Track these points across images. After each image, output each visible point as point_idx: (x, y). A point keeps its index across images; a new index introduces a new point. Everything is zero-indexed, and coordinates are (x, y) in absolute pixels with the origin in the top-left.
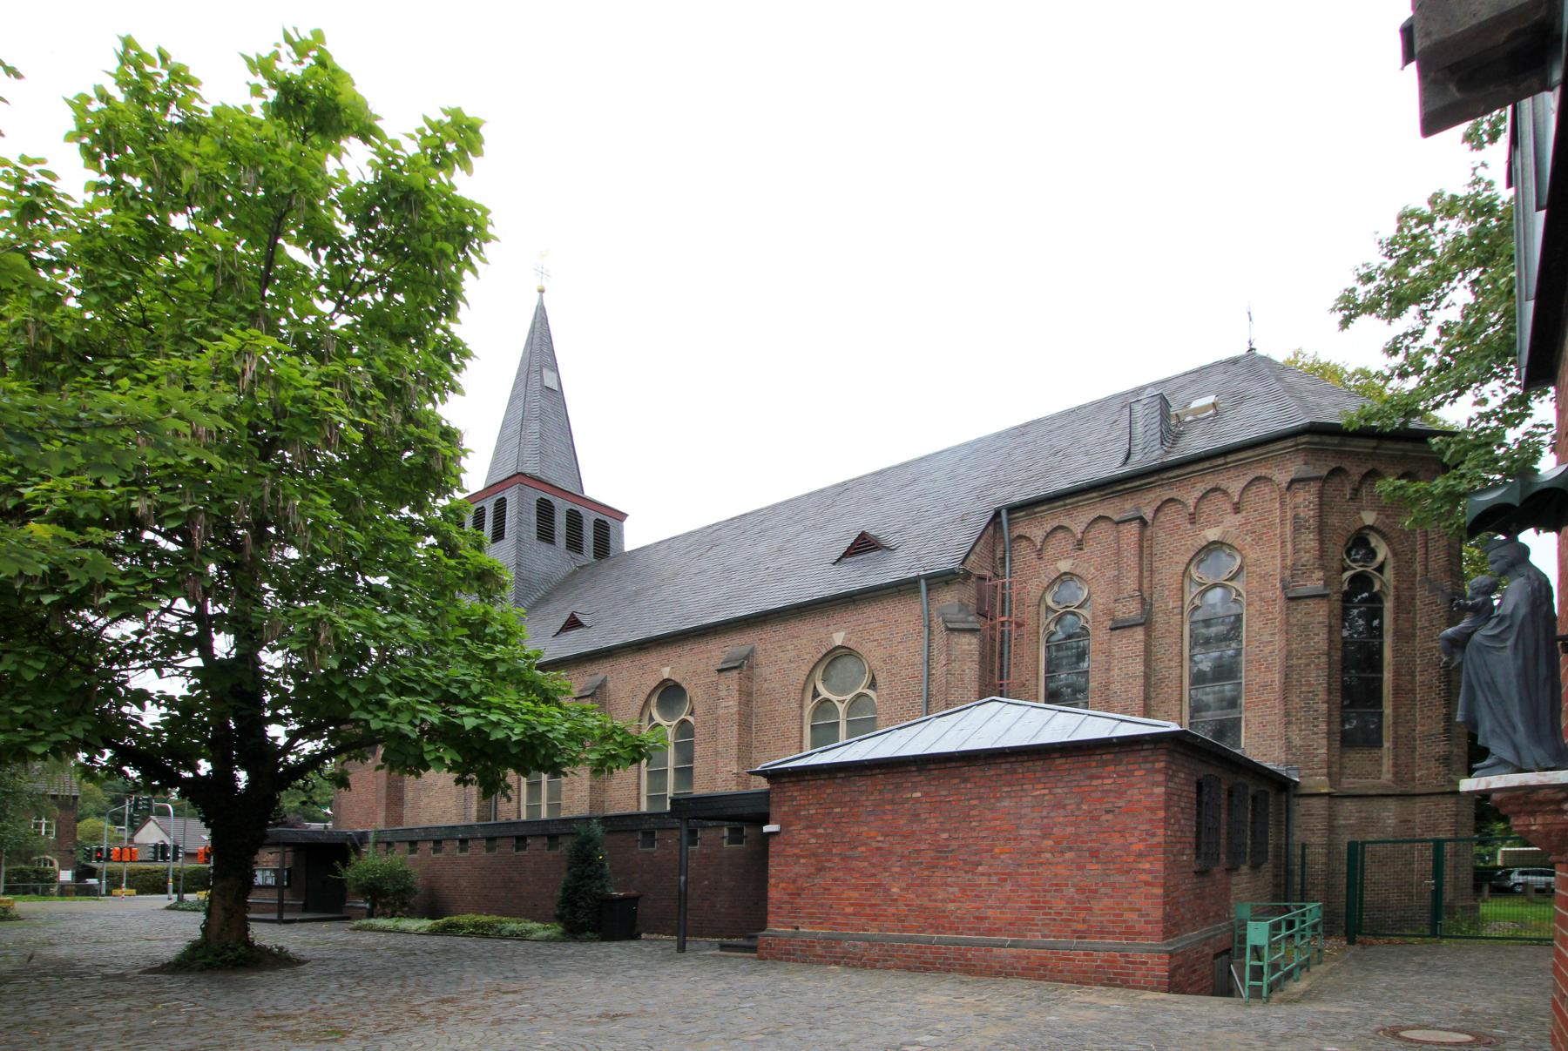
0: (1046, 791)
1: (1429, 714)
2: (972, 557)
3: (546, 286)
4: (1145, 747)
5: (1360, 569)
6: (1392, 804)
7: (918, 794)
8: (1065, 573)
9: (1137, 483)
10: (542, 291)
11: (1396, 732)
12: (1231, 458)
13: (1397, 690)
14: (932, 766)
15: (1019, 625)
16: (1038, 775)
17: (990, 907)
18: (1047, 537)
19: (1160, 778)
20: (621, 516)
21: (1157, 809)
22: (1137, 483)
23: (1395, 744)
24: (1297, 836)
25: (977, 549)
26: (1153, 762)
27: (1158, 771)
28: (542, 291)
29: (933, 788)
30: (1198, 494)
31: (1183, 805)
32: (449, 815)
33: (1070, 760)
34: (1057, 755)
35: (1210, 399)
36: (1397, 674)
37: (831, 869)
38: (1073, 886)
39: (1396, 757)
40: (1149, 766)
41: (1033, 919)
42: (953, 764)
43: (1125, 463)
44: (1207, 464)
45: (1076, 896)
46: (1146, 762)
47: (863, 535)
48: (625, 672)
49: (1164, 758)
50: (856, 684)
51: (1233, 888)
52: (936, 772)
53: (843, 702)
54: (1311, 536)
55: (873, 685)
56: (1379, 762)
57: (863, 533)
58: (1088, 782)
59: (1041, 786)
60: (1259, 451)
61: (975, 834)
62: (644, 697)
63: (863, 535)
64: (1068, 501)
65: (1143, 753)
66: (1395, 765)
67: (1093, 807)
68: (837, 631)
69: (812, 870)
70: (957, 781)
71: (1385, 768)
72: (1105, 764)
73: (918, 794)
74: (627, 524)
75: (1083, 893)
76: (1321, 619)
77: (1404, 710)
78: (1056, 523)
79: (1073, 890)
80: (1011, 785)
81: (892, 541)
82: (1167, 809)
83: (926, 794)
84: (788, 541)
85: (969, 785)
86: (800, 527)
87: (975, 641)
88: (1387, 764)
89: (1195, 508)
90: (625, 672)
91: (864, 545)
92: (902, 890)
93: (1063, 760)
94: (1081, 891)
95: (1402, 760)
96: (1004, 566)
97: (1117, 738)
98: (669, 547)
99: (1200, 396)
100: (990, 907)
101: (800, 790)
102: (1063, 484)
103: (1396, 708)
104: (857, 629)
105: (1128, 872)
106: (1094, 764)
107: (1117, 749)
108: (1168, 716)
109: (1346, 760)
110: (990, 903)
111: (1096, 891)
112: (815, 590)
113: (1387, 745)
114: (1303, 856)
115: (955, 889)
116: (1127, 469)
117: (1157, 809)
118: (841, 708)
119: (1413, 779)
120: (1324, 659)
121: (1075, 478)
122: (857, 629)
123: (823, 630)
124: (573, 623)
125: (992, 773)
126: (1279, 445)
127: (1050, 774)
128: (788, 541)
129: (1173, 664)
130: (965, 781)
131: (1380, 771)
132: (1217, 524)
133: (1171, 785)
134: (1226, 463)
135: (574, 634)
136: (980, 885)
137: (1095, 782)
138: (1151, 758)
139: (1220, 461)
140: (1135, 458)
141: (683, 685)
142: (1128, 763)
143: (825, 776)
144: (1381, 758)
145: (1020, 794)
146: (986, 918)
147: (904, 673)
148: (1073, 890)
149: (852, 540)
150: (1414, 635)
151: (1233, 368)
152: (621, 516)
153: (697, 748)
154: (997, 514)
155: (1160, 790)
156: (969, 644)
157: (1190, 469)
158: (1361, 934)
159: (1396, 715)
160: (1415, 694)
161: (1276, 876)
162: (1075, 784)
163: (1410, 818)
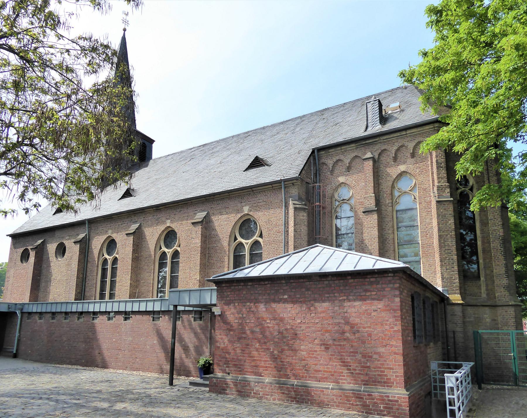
0: (345, 298)
1: (498, 263)
2: (303, 172)
3: (126, 27)
4: (389, 275)
5: (464, 189)
6: (487, 310)
7: (286, 297)
8: (342, 183)
9: (396, 135)
10: (125, 30)
11: (485, 272)
12: (408, 132)
13: (484, 251)
14: (292, 281)
15: (323, 208)
16: (341, 288)
17: (321, 365)
18: (334, 164)
19: (397, 293)
20: (152, 141)
21: (397, 310)
22: (371, 141)
23: (486, 278)
24: (450, 326)
25: (305, 168)
26: (394, 284)
27: (396, 289)
28: (125, 30)
29: (293, 293)
30: (395, 148)
31: (407, 308)
32: (61, 297)
33: (356, 280)
34: (349, 277)
35: (397, 104)
36: (483, 243)
37: (245, 338)
38: (361, 353)
39: (487, 285)
40: (391, 285)
41: (342, 373)
42: (302, 280)
43: (366, 131)
44: (398, 134)
45: (363, 360)
46: (391, 284)
47: (257, 158)
48: (150, 222)
49: (398, 281)
50: (253, 235)
51: (429, 356)
52: (294, 284)
53: (247, 244)
54: (443, 172)
55: (261, 236)
56: (479, 287)
57: (257, 157)
58: (364, 294)
59: (343, 294)
60: (419, 129)
61: (313, 321)
62: (158, 236)
63: (257, 158)
64: (343, 148)
65: (389, 278)
66: (487, 290)
67: (367, 308)
68: (245, 205)
69: (236, 339)
70: (304, 290)
71: (482, 291)
72: (371, 283)
73: (286, 297)
74: (154, 145)
75: (365, 358)
76: (450, 213)
77: (488, 261)
78: (338, 158)
79: (360, 355)
80: (329, 294)
81: (269, 161)
82: (401, 311)
83: (290, 296)
84: (224, 159)
85: (309, 293)
86: (229, 152)
87: (305, 214)
88: (483, 289)
89: (395, 155)
90: (150, 222)
91: (257, 163)
92: (279, 352)
93: (352, 280)
94: (364, 356)
95: (490, 287)
96: (317, 177)
97: (377, 269)
98: (172, 158)
99: (394, 102)
100: (321, 365)
101: (231, 292)
102: (340, 139)
103: (484, 260)
104: (254, 205)
105: (385, 346)
106: (367, 283)
107: (377, 276)
108: (399, 258)
109: (466, 286)
110: (321, 362)
111: (371, 357)
112: (235, 184)
113: (482, 279)
114: (454, 337)
115: (305, 353)
116: (366, 133)
117: (397, 310)
118: (247, 247)
119: (495, 298)
120: (453, 233)
121: (345, 137)
122: (254, 205)
123: (239, 205)
124: (128, 194)
125: (320, 286)
126: (427, 127)
127: (347, 288)
128: (224, 159)
129: (390, 232)
130: (308, 290)
131: (481, 293)
132: (404, 163)
133: (402, 296)
134: (406, 134)
135: (127, 200)
136: (316, 351)
137: (368, 294)
138: (393, 281)
139: (404, 133)
140: (369, 129)
141: (176, 230)
142: (382, 284)
143: (242, 284)
144: (480, 285)
145: (334, 299)
146: (320, 371)
147: (275, 229)
148: (360, 355)
149: (252, 160)
150: (488, 223)
151: (405, 90)
152: (152, 141)
153: (180, 265)
154: (313, 152)
155: (398, 300)
156: (303, 216)
157: (392, 136)
158: (484, 383)
159: (485, 264)
160: (491, 253)
161: (443, 349)
162: (358, 294)
163: (496, 318)
